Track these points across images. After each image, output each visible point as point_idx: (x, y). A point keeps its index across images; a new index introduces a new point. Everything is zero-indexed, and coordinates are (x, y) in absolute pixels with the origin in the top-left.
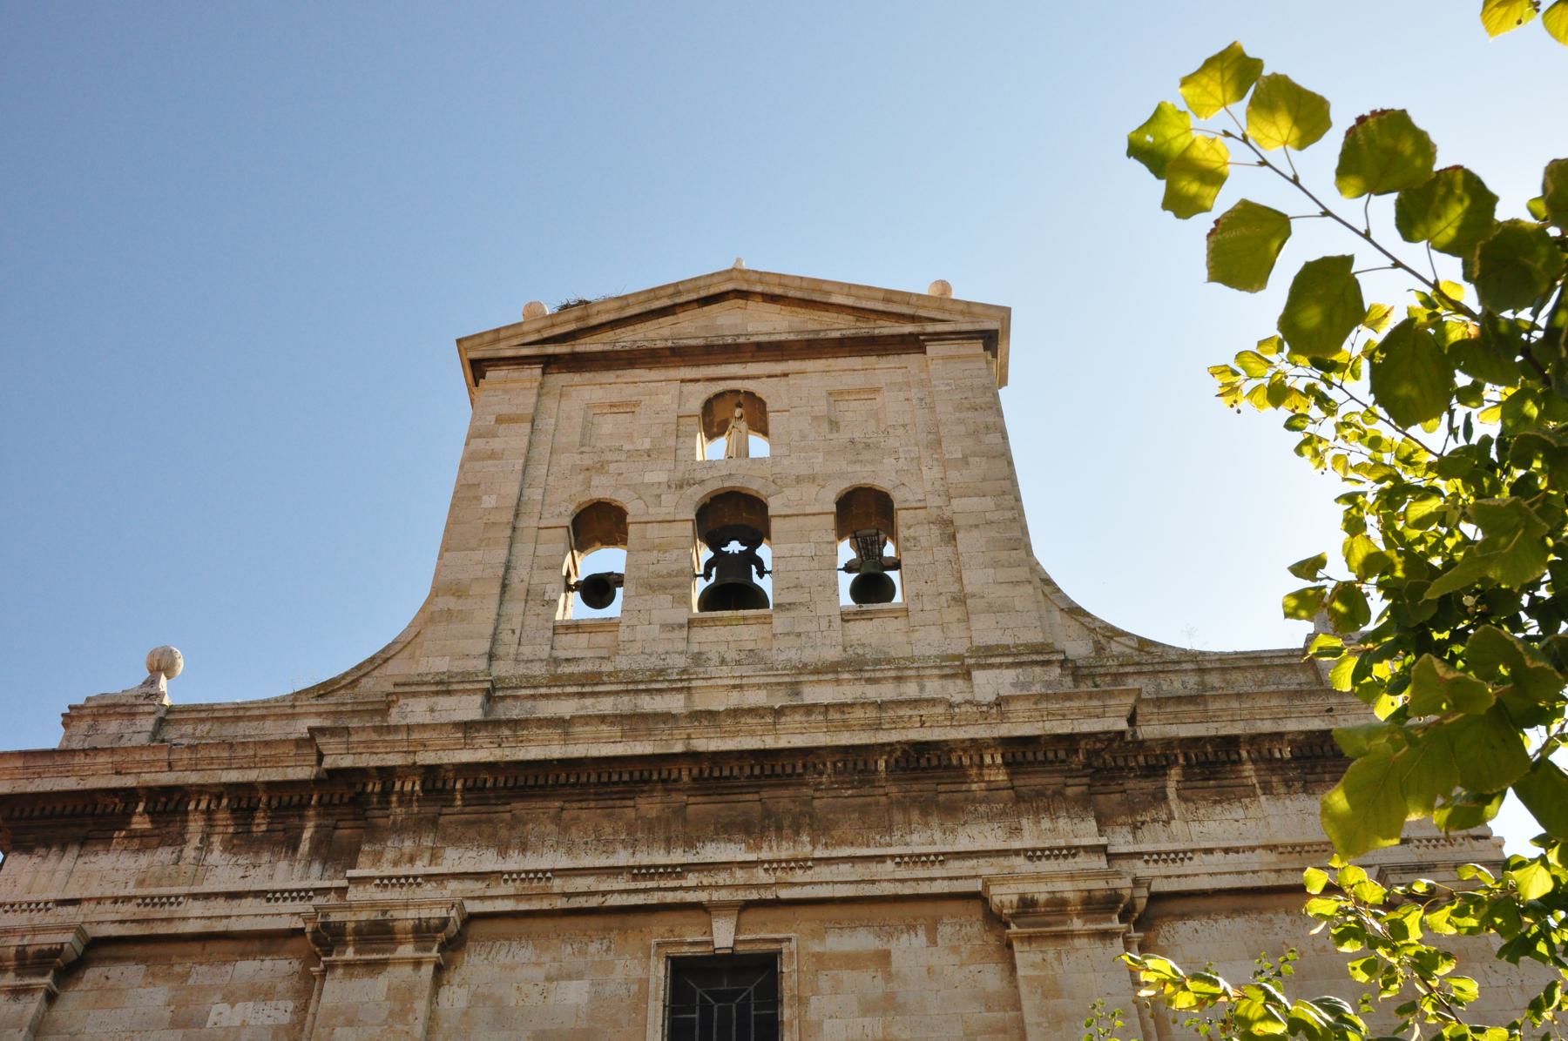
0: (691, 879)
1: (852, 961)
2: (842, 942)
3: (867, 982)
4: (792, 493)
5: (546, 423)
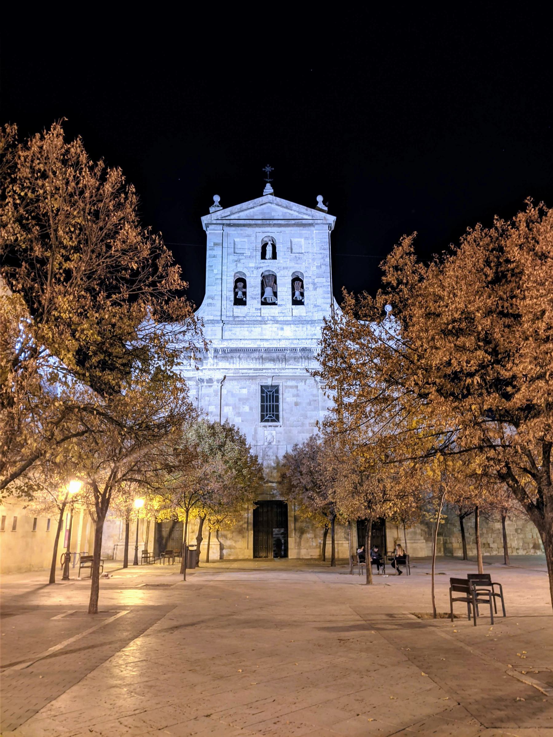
0: (264, 371)
1: (291, 387)
2: (290, 383)
3: (294, 391)
4: (282, 272)
5: (225, 245)
